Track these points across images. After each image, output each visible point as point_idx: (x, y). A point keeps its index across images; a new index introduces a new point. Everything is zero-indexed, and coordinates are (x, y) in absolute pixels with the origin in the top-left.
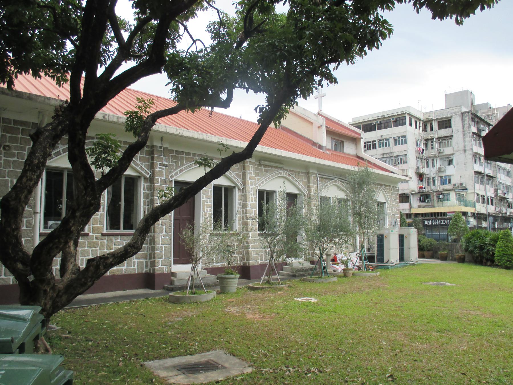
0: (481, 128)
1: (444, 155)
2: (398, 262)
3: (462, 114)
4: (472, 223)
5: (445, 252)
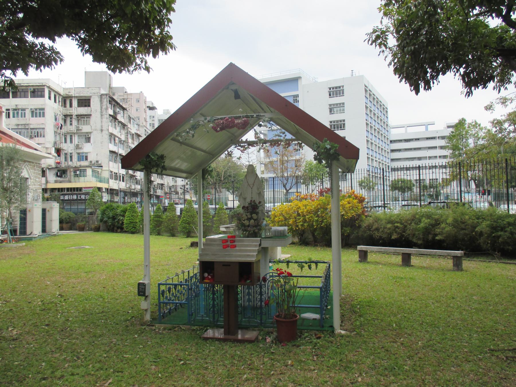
0: (117, 111)
1: (82, 133)
2: (41, 234)
3: (101, 95)
4: (106, 198)
5: (83, 223)
